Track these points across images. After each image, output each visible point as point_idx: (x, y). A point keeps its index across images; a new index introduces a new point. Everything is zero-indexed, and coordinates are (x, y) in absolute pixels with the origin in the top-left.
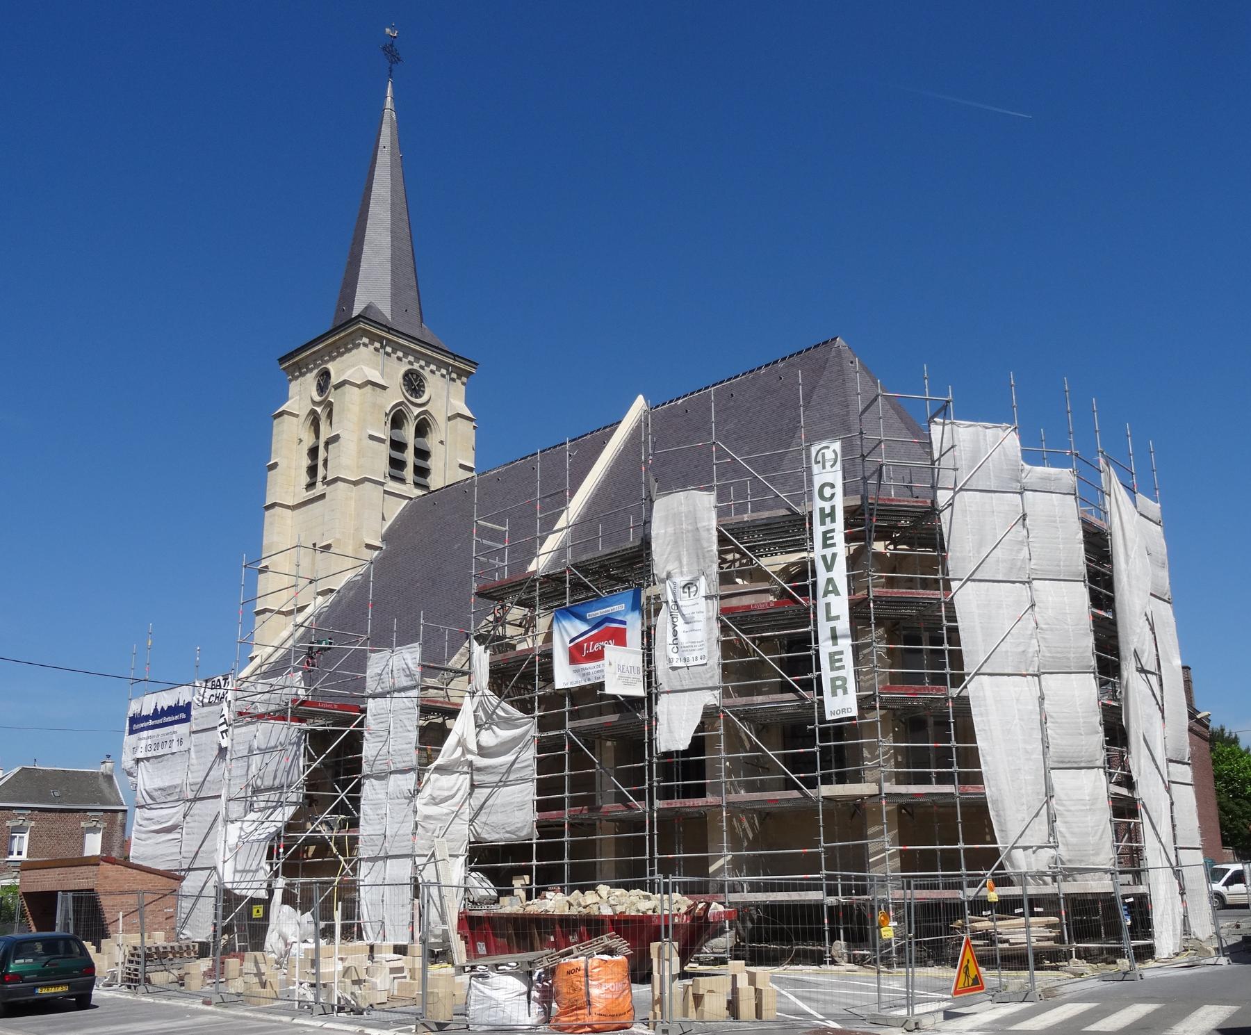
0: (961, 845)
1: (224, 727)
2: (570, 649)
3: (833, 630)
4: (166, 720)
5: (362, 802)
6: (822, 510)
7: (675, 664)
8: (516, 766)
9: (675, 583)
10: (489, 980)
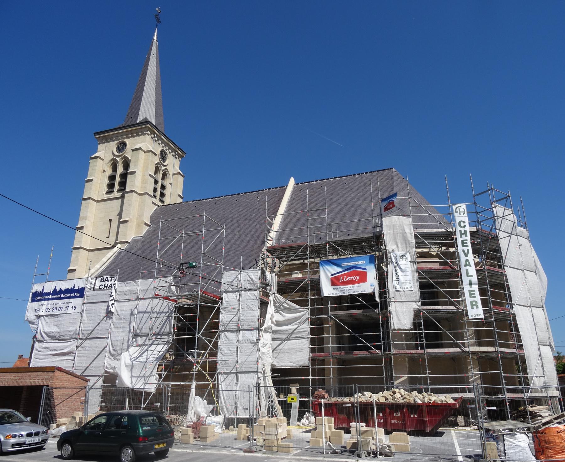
0: (428, 375)
1: (113, 302)
2: (331, 279)
3: (470, 281)
4: (62, 296)
5: (219, 344)
7: (398, 289)
10: (516, 436)
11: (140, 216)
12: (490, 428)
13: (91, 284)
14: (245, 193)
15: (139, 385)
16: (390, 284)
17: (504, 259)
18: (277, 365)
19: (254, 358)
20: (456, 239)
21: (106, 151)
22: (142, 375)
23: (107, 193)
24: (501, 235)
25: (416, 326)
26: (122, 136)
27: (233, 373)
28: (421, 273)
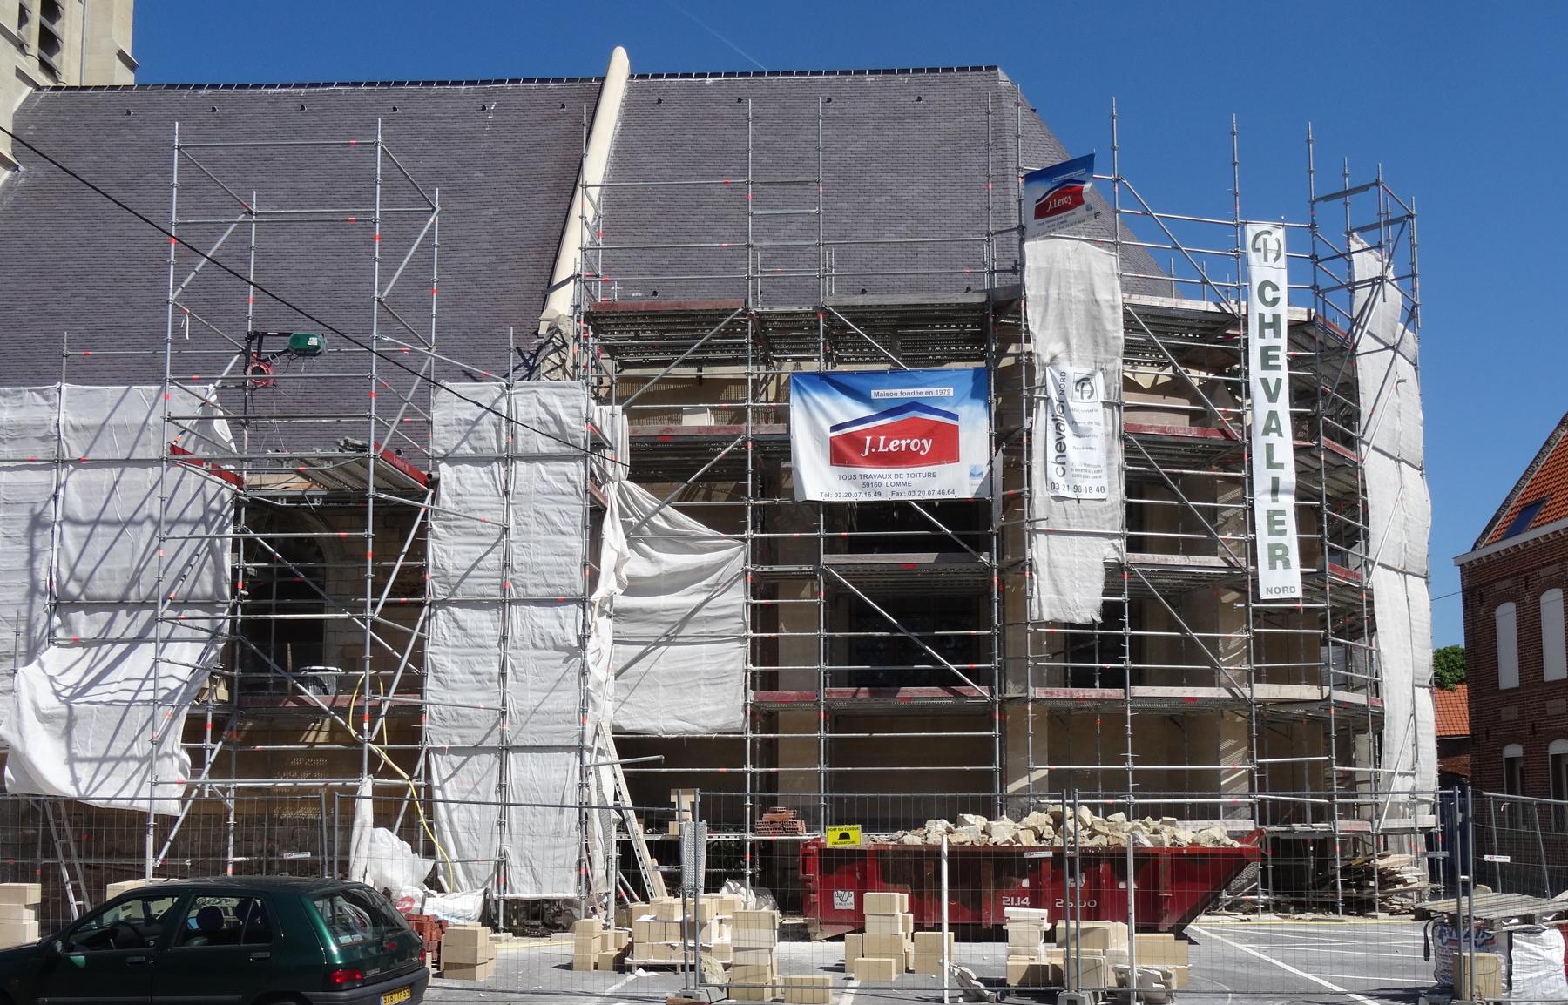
3: (1275, 481)
6: (1262, 316)
7: (1062, 493)
8: (702, 613)
9: (1063, 374)
12: (1494, 915)
14: (426, 83)
15: (112, 789)
16: (1037, 473)
17: (1363, 421)
18: (628, 725)
19: (567, 700)
20: (1246, 340)
22: (117, 750)
24: (1365, 343)
25: (1110, 612)
27: (489, 750)
28: (1135, 445)
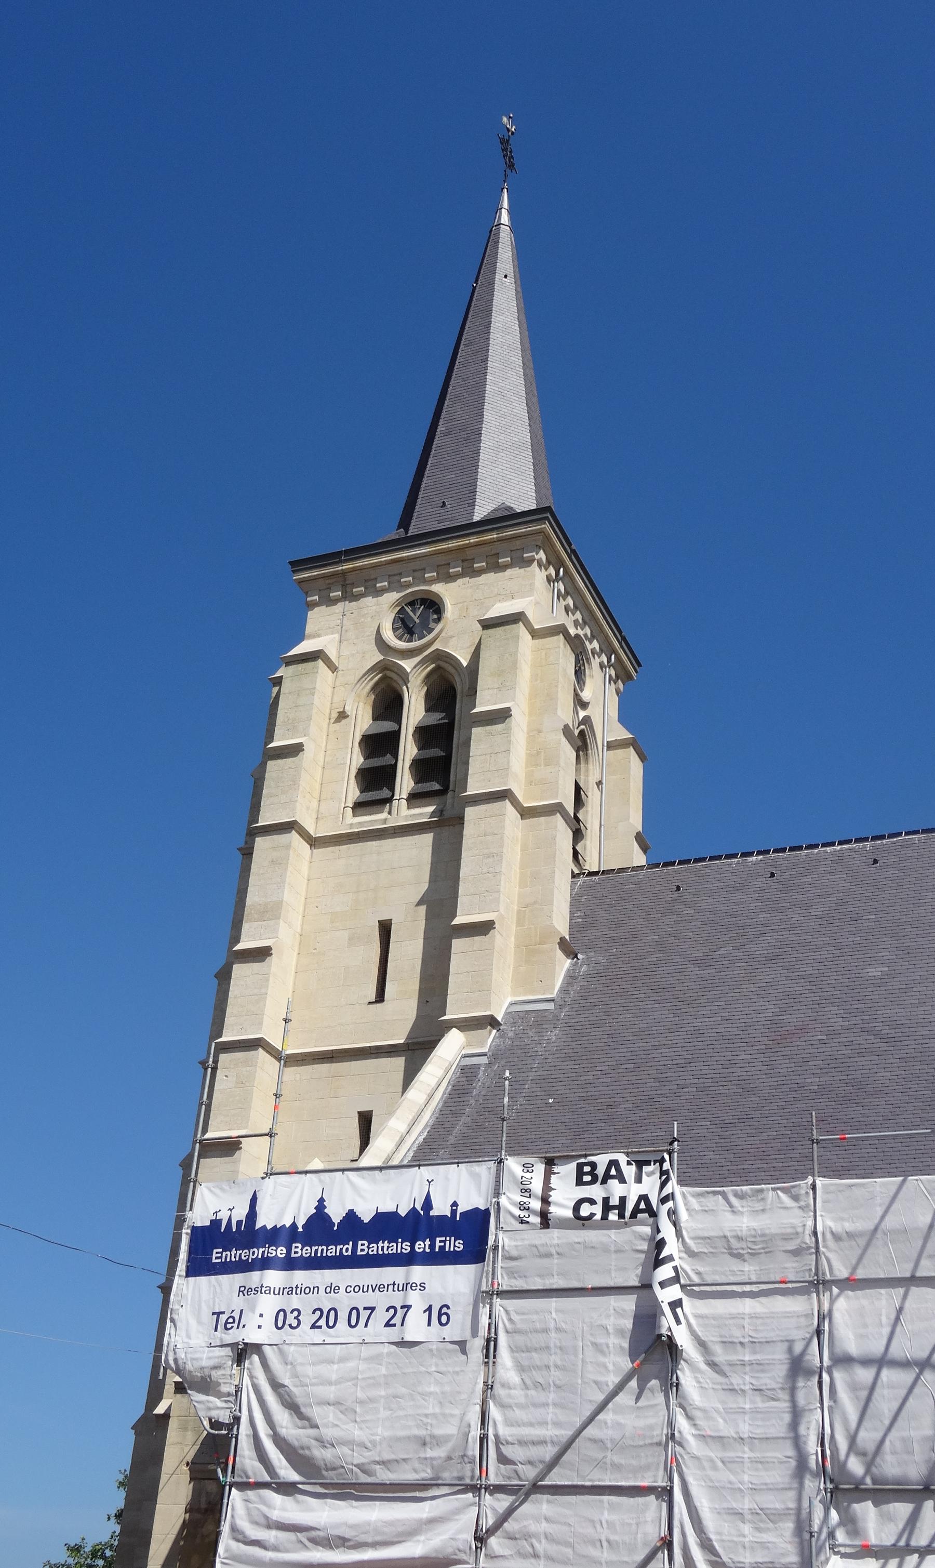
4: (363, 1247)
11: (532, 908)
13: (526, 1191)
21: (346, 636)
23: (360, 807)
26: (419, 575)
